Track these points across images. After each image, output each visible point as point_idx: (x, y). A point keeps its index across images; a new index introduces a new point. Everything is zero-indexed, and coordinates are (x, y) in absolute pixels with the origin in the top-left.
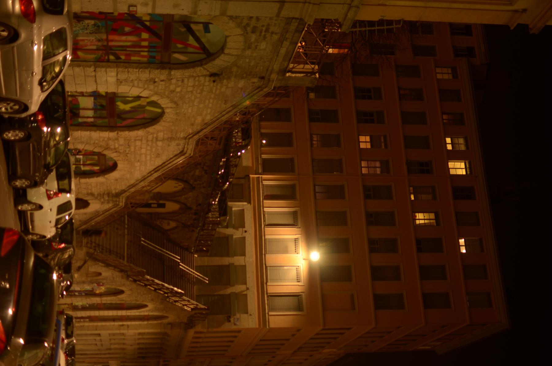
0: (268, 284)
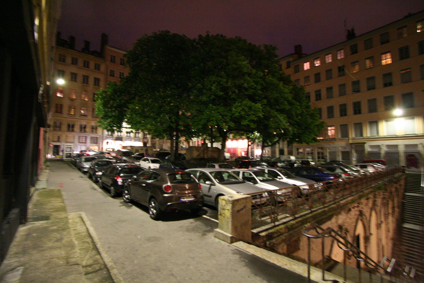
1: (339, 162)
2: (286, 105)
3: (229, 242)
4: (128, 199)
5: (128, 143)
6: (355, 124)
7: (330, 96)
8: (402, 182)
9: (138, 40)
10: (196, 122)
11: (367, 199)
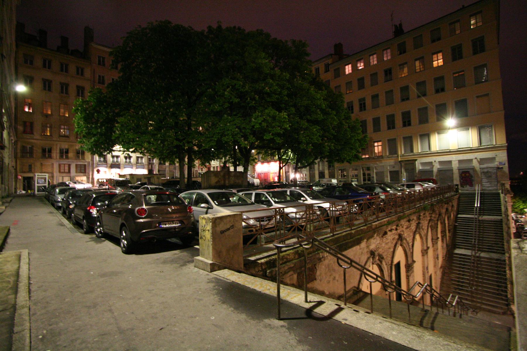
0: (471, 147)
2: (319, 114)
3: (209, 270)
4: (100, 232)
5: (127, 171)
7: (376, 106)
8: (455, 203)
9: (128, 33)
10: (207, 137)
11: (409, 221)
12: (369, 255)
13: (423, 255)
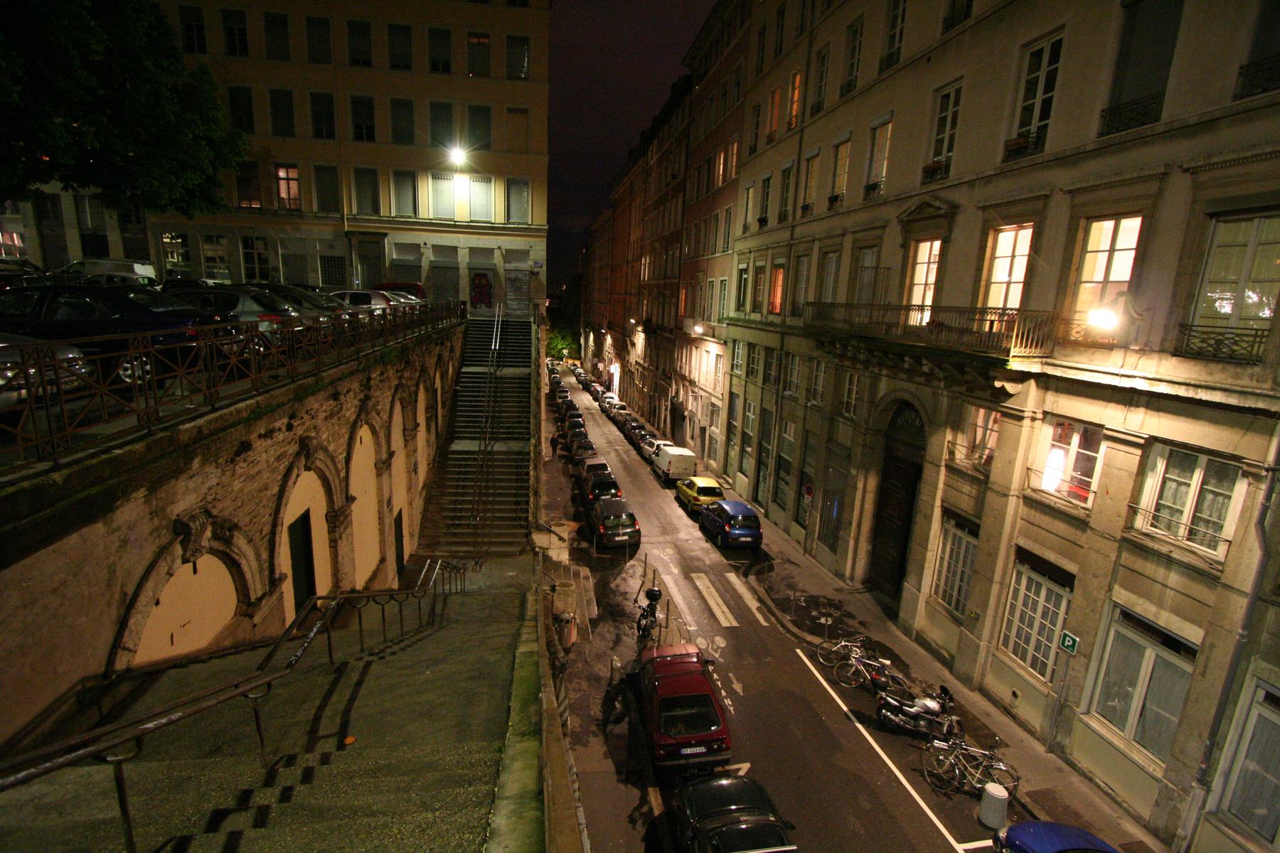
1: (314, 289)
6: (359, 172)
11: (335, 397)
12: (166, 536)
13: (379, 475)
